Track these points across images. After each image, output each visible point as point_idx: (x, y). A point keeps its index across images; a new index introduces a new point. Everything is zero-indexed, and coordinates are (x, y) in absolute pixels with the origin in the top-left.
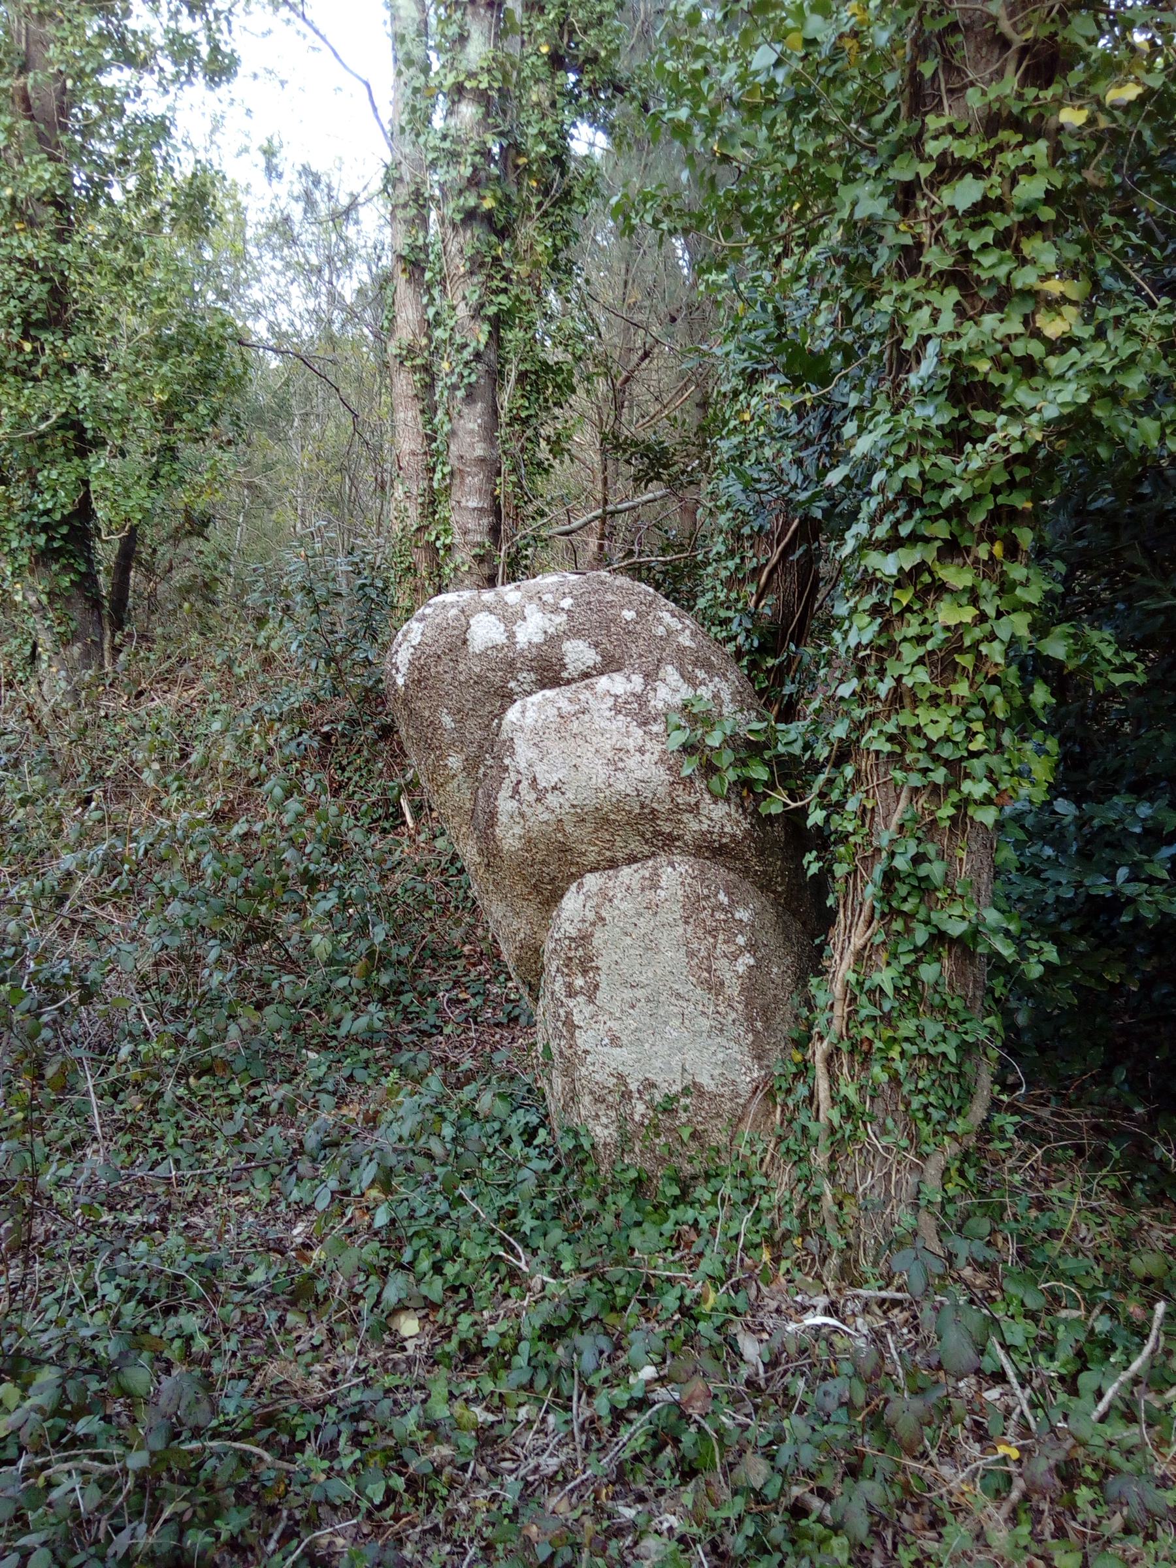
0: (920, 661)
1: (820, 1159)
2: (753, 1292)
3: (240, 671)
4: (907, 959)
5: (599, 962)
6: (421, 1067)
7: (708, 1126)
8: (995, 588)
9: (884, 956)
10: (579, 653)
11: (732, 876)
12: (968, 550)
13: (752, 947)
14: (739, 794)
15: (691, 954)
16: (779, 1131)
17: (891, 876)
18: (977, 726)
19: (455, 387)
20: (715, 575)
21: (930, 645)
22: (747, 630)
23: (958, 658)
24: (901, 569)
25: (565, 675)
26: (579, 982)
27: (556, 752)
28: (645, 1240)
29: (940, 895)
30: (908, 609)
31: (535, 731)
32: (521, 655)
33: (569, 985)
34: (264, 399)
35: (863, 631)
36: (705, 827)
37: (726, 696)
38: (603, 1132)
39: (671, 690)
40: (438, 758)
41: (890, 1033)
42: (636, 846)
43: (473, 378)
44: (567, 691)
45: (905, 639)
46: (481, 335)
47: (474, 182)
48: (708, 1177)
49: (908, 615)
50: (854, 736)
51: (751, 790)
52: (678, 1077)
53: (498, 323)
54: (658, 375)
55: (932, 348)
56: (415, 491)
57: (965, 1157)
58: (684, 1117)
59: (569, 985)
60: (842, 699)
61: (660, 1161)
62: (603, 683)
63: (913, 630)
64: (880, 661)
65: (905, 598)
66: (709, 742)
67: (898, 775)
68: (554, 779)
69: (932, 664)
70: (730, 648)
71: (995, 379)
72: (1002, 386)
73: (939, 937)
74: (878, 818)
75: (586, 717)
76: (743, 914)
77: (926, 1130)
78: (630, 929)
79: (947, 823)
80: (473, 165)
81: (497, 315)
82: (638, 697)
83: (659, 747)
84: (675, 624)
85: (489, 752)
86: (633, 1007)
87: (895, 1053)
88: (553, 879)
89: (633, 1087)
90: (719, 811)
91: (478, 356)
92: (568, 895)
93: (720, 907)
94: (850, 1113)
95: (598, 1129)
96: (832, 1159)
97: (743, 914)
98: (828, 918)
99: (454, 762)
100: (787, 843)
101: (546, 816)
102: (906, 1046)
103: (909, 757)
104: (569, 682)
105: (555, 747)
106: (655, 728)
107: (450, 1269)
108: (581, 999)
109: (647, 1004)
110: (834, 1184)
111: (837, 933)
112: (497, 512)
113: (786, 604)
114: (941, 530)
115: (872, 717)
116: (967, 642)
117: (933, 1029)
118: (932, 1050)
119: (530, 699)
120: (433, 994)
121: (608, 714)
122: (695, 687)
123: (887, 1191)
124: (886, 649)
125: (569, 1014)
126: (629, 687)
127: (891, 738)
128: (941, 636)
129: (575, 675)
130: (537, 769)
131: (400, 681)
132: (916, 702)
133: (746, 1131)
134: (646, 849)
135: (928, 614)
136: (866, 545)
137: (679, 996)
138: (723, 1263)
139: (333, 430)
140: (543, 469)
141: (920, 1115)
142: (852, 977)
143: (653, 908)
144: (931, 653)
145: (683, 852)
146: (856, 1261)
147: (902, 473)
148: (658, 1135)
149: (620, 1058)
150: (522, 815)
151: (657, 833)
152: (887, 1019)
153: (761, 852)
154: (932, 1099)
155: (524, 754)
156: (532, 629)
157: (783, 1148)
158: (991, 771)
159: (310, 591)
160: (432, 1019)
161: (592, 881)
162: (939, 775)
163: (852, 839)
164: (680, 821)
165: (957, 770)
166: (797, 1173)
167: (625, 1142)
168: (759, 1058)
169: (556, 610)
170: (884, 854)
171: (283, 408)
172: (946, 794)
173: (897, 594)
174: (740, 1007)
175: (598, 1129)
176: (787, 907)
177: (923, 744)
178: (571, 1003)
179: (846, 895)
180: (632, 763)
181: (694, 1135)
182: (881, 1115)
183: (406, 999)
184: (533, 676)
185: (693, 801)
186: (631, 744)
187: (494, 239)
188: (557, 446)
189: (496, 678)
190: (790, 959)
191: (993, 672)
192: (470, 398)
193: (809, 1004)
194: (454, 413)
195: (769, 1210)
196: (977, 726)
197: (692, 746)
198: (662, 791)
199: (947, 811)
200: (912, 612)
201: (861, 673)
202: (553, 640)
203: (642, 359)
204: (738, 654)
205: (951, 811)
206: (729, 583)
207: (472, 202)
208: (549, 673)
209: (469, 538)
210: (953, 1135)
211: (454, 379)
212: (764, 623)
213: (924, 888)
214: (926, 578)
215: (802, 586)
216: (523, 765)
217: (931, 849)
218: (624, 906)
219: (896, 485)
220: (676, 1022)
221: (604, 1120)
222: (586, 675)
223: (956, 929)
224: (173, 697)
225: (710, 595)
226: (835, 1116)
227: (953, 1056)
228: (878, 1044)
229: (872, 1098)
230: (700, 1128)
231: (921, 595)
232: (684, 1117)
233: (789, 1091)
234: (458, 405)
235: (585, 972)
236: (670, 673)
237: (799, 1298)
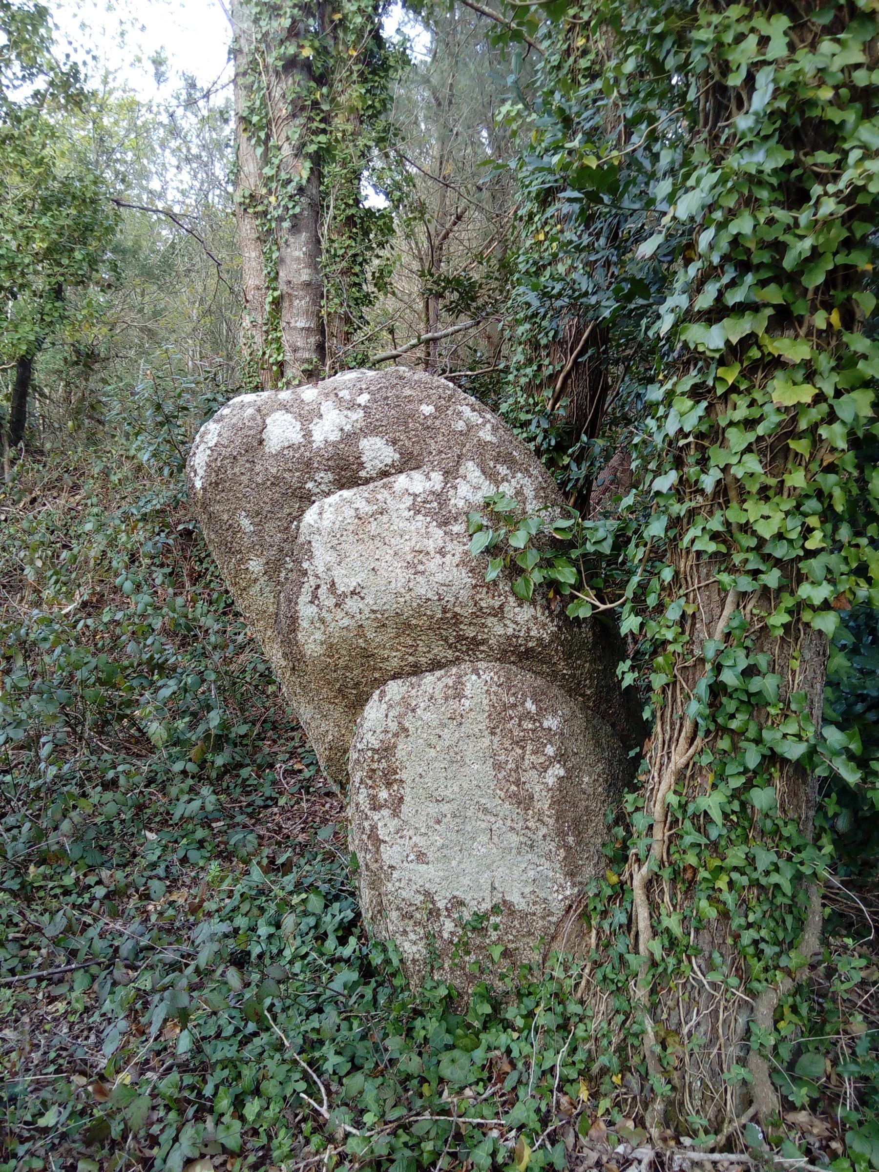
0: (749, 449)
1: (640, 994)
2: (571, 1140)
3: (114, 479)
4: (737, 782)
5: (403, 775)
6: (250, 848)
7: (520, 945)
8: (833, 363)
9: (711, 778)
10: (376, 451)
11: (539, 682)
12: (800, 320)
13: (561, 757)
14: (545, 596)
15: (498, 766)
16: (595, 957)
17: (717, 690)
18: (813, 521)
19: (280, 219)
20: (516, 383)
21: (760, 430)
22: (545, 431)
23: (793, 444)
24: (728, 342)
25: (363, 474)
26: (383, 794)
27: (354, 555)
28: (457, 1067)
29: (773, 711)
30: (734, 389)
31: (332, 533)
33: (373, 798)
34: (154, 259)
35: (685, 416)
36: (510, 631)
37: (529, 493)
38: (412, 948)
39: (471, 488)
40: (240, 562)
41: (718, 862)
42: (440, 651)
43: (297, 210)
44: (364, 491)
45: (731, 424)
46: (303, 171)
47: (293, 32)
48: (520, 995)
49: (734, 397)
50: (671, 534)
51: (557, 592)
52: (487, 895)
53: (319, 159)
54: (470, 234)
55: (764, 80)
56: (260, 321)
57: (798, 990)
58: (494, 935)
59: (373, 798)
60: (658, 493)
61: (471, 978)
62: (401, 481)
63: (741, 413)
64: (702, 449)
65: (731, 375)
66: (513, 542)
67: (725, 578)
69: (760, 452)
70: (532, 446)
71: (834, 115)
72: (843, 122)
73: (772, 758)
74: (697, 626)
75: (385, 518)
76: (551, 722)
77: (757, 966)
78: (434, 740)
79: (781, 632)
80: (292, 17)
81: (316, 152)
82: (438, 495)
83: (460, 549)
84: (475, 418)
85: (288, 556)
86: (439, 822)
87: (722, 883)
88: (357, 684)
89: (441, 905)
90: (525, 614)
91: (301, 190)
92: (371, 703)
93: (527, 716)
94: (672, 944)
95: (407, 945)
96: (653, 991)
97: (551, 722)
98: (645, 731)
99: (255, 565)
100: (595, 644)
101: (346, 622)
102: (735, 876)
103: (737, 558)
104: (367, 481)
105: (353, 550)
106: (456, 528)
107: (252, 1108)
108: (386, 812)
109: (452, 817)
110: (656, 1021)
111: (654, 748)
112: (321, 330)
113: (579, 407)
114: (774, 295)
115: (692, 513)
116: (803, 425)
117: (765, 859)
118: (763, 881)
119: (328, 500)
120: (271, 766)
121: (407, 514)
122: (497, 483)
123: (715, 1030)
124: (711, 435)
125: (374, 828)
126: (428, 485)
127: (715, 536)
128: (774, 419)
130: (335, 573)
131: (198, 484)
132: (743, 495)
133: (559, 950)
134: (450, 654)
135: (757, 395)
136: (687, 317)
137: (486, 811)
138: (538, 1111)
139: (206, 283)
140: (368, 301)
141: (751, 950)
142: (673, 800)
143: (457, 718)
144: (759, 439)
145: (488, 658)
146: (682, 1104)
147: (733, 228)
148: (468, 953)
149: (428, 875)
150: (322, 621)
151: (461, 638)
152: (714, 846)
153: (568, 656)
154: (763, 933)
155: (322, 558)
156: (328, 427)
157: (599, 976)
158: (829, 571)
159: (158, 407)
160: (268, 791)
161: (394, 689)
162: (772, 578)
163: (670, 648)
164: (484, 625)
165: (793, 574)
166: (615, 1003)
167: (434, 958)
168: (571, 874)
169: (353, 406)
170: (708, 666)
171: (167, 265)
172: (777, 597)
173: (721, 372)
174: (551, 821)
175: (407, 945)
176: (596, 710)
177: (753, 543)
178: (376, 816)
179: (663, 708)
180: (432, 565)
181: (506, 954)
182: (707, 948)
183: (245, 772)
184: (330, 476)
185: (497, 604)
186: (431, 545)
187: (313, 84)
188: (381, 281)
189: (293, 478)
190: (600, 767)
191: (828, 459)
192: (295, 229)
193: (622, 819)
194: (282, 242)
195: (585, 1040)
196: (813, 521)
197: (496, 547)
198: (464, 595)
199: (779, 619)
200: (739, 393)
201: (679, 463)
202: (350, 438)
203: (455, 224)
204: (538, 453)
205: (786, 618)
206: (530, 389)
207: (291, 50)
208: (347, 473)
209: (298, 355)
210: (788, 972)
211: (280, 211)
212: (559, 424)
213: (754, 703)
214: (755, 353)
215: (593, 389)
216: (321, 569)
217: (762, 661)
218: (427, 716)
219: (724, 245)
220: (484, 838)
221: (412, 936)
222: (384, 474)
223: (794, 751)
224: (61, 502)
225: (511, 401)
226: (656, 947)
227: (787, 888)
228: (703, 874)
229: (697, 930)
230: (511, 946)
231: (748, 373)
232: (494, 935)
233: (604, 914)
234: (284, 235)
235: (389, 785)
236: (471, 469)
237: (620, 1149)
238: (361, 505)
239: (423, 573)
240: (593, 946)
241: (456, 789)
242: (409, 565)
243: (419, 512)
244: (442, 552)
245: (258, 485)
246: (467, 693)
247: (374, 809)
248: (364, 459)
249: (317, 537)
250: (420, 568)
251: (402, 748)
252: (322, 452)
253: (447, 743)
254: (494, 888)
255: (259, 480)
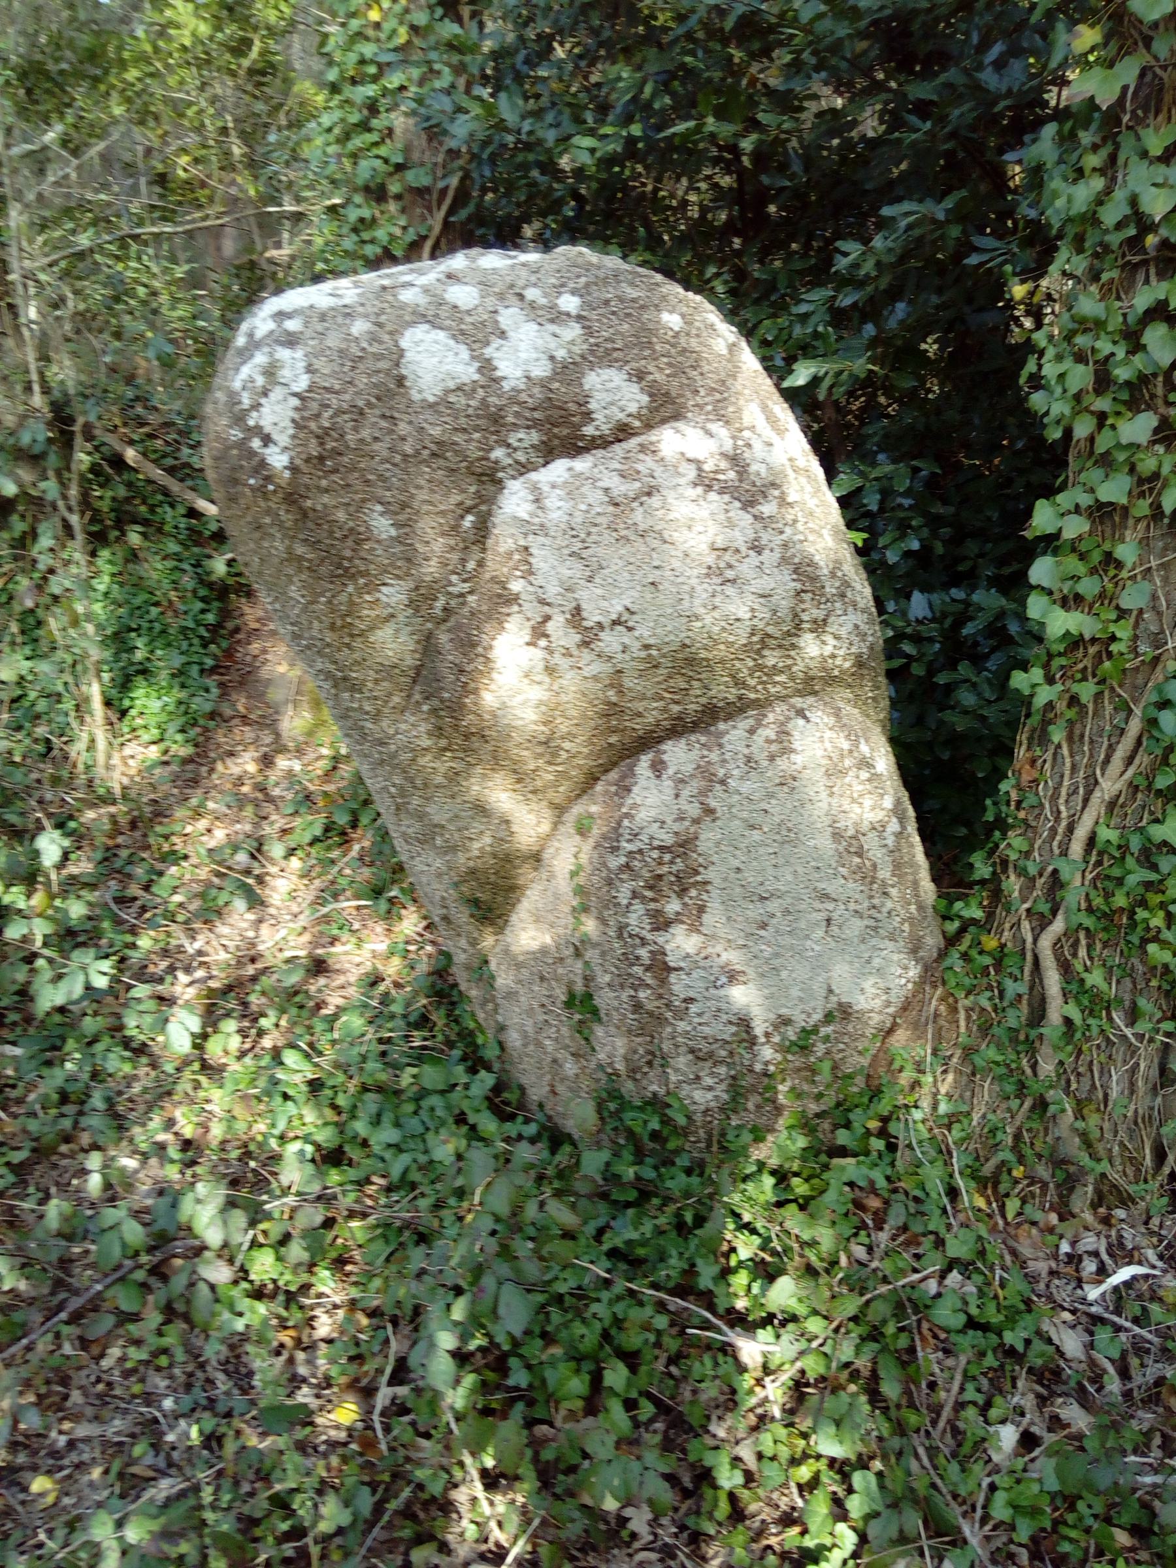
5: (710, 874)
10: (612, 393)
25: (589, 430)
26: (673, 906)
32: (513, 400)
36: (828, 650)
40: (360, 591)
68: (616, 608)
75: (655, 501)
78: (758, 818)
86: (764, 926)
105: (605, 550)
129: (606, 429)
156: (524, 354)
169: (559, 317)
180: (746, 568)
184: (535, 437)
202: (568, 371)
208: (563, 429)
218: (746, 787)
221: (709, 1081)
232: (820, 1049)
235: (682, 892)
238: (613, 482)
239: (733, 581)
240: (963, 1029)
241: (790, 878)
242: (710, 571)
243: (709, 488)
244: (757, 548)
245: (405, 456)
246: (796, 745)
247: (657, 929)
248: (593, 405)
249: (541, 539)
250: (730, 574)
251: (708, 837)
252: (523, 397)
253: (777, 819)
254: (831, 991)
255: (408, 449)
